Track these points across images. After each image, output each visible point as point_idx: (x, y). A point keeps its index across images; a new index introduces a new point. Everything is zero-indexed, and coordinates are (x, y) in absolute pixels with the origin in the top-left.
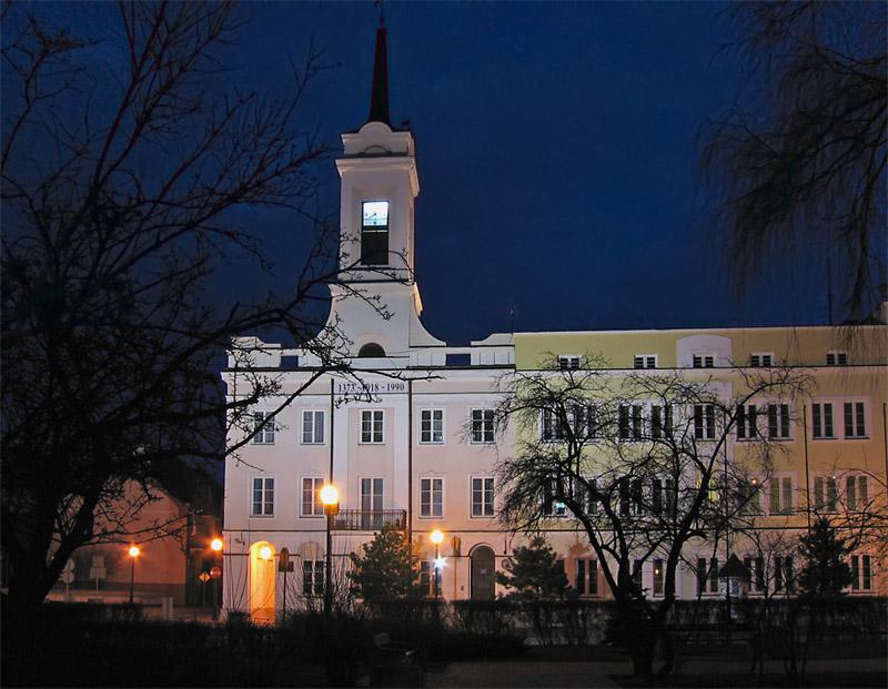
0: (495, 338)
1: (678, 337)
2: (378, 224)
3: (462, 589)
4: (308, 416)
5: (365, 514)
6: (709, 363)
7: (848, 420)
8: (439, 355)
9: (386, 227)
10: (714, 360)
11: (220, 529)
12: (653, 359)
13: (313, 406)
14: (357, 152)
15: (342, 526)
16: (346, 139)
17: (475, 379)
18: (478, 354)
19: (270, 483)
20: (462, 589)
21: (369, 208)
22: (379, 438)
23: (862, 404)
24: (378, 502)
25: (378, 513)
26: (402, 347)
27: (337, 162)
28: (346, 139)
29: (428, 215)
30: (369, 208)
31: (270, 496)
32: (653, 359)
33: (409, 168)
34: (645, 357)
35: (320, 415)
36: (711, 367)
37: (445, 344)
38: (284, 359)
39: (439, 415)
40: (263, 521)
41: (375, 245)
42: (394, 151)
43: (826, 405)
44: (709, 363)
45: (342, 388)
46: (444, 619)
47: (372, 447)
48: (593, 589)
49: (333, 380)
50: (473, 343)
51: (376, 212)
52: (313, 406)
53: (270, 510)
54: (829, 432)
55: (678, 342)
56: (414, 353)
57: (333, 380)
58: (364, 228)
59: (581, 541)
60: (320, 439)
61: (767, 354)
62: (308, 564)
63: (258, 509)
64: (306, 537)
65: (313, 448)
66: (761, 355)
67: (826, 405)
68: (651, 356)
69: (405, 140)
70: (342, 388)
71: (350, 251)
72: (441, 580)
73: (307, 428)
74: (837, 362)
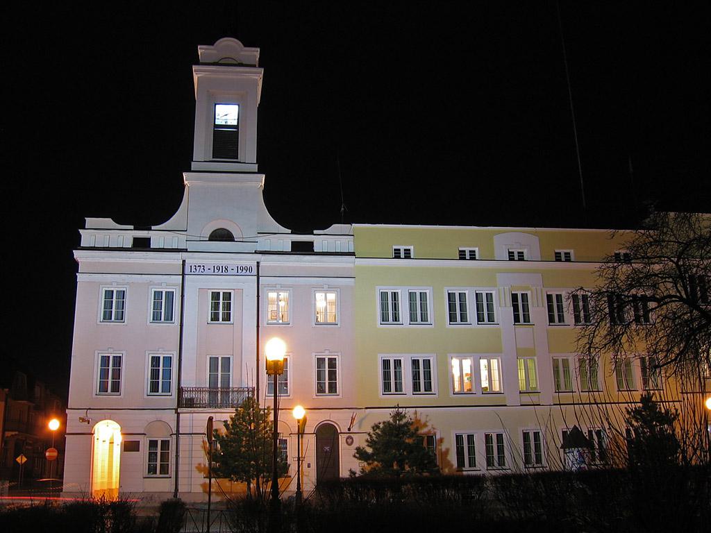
0: (336, 228)
1: (499, 232)
2: (229, 123)
3: (309, 466)
4: (158, 295)
5: (213, 391)
6: (521, 257)
7: (479, 308)
8: (286, 239)
9: (236, 127)
10: (477, 253)
11: (61, 408)
12: (474, 251)
13: (114, 284)
14: (212, 62)
15: (190, 403)
16: (202, 50)
17: (318, 265)
18: (320, 240)
19: (118, 361)
20: (309, 466)
21: (221, 109)
22: (227, 318)
23: (491, 294)
24: (226, 379)
25: (226, 390)
26: (250, 233)
27: (194, 68)
28: (202, 50)
29: (272, 115)
30: (221, 109)
31: (117, 374)
32: (474, 251)
33: (258, 76)
34: (402, 248)
35: (170, 295)
36: (523, 260)
37: (290, 231)
38: (136, 240)
39: (122, 294)
40: (110, 399)
41: (225, 142)
42: (244, 63)
43: (522, 294)
44: (521, 257)
45: (193, 269)
46: (83, 501)
47: (221, 326)
48: (472, 463)
49: (184, 261)
50: (315, 232)
51: (227, 114)
52: (114, 284)
53: (116, 388)
54: (463, 318)
55: (495, 238)
56: (261, 239)
57: (184, 261)
58: (216, 126)
59: (418, 418)
60: (169, 317)
61: (568, 251)
62: (153, 444)
63: (103, 388)
64: (150, 416)
65: (163, 326)
66: (562, 251)
67: (522, 294)
68: (407, 248)
69: (255, 53)
70: (193, 269)
71: (202, 145)
72: (450, 453)
73: (157, 306)
74: (402, 255)
